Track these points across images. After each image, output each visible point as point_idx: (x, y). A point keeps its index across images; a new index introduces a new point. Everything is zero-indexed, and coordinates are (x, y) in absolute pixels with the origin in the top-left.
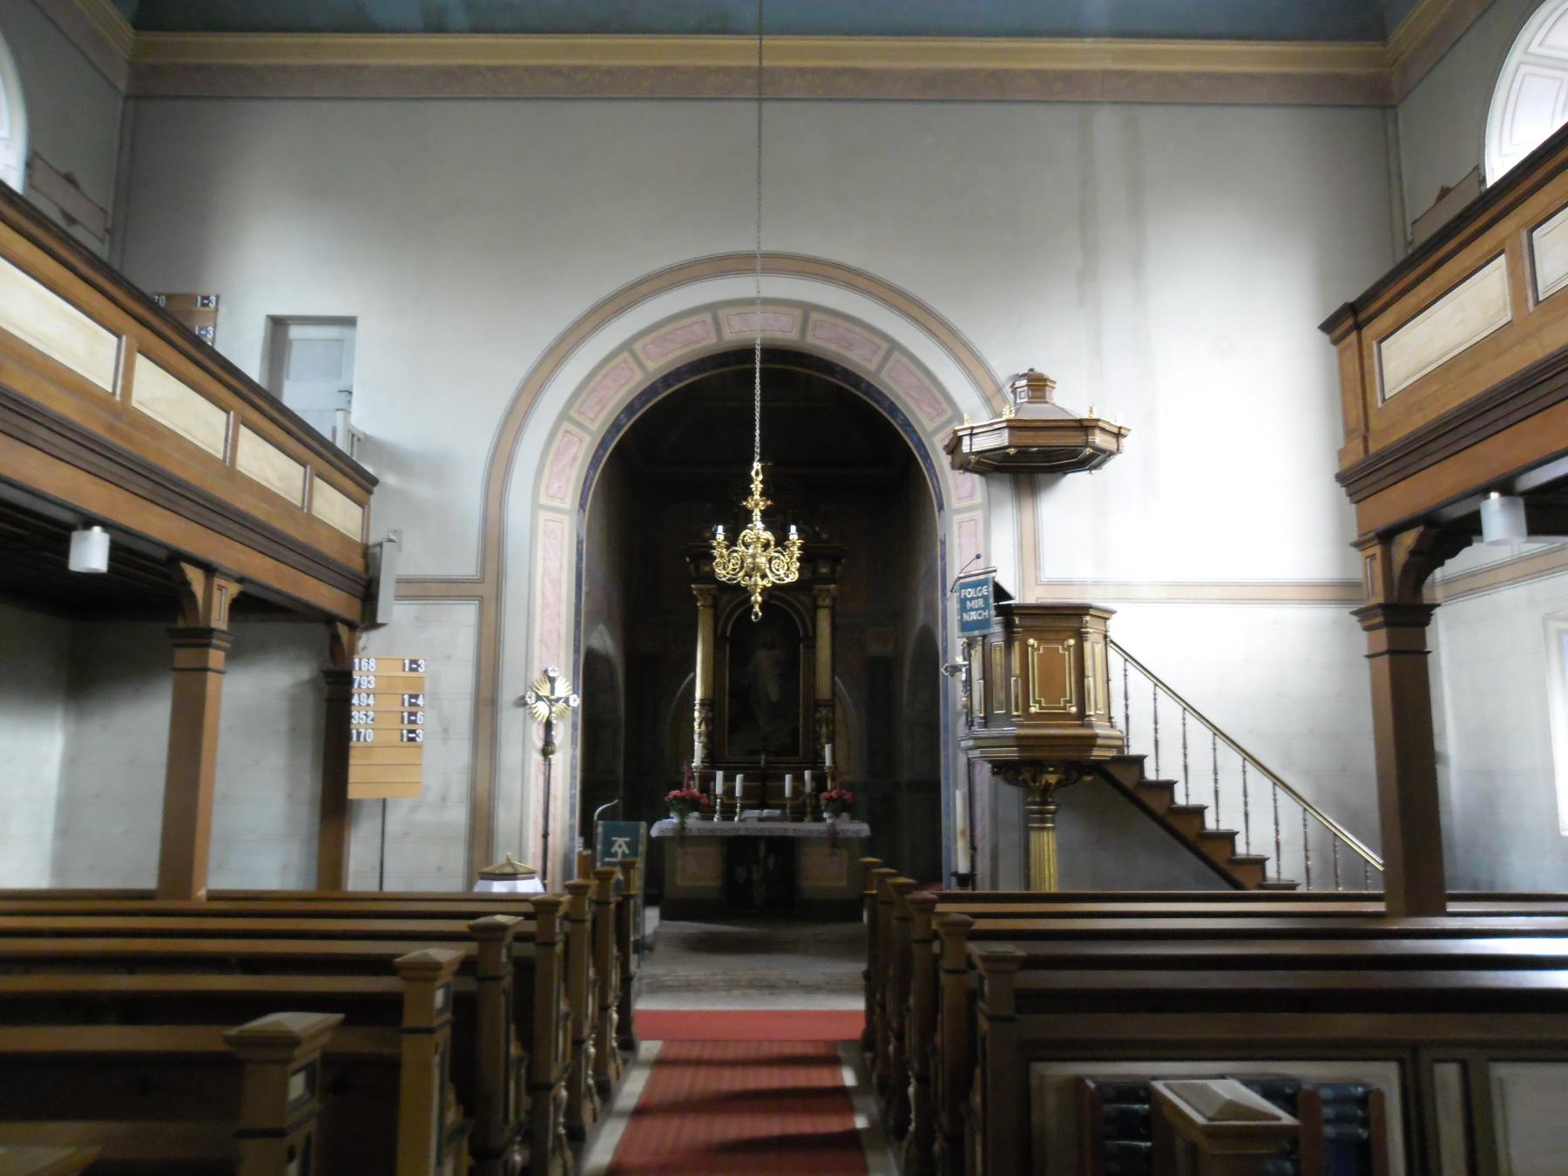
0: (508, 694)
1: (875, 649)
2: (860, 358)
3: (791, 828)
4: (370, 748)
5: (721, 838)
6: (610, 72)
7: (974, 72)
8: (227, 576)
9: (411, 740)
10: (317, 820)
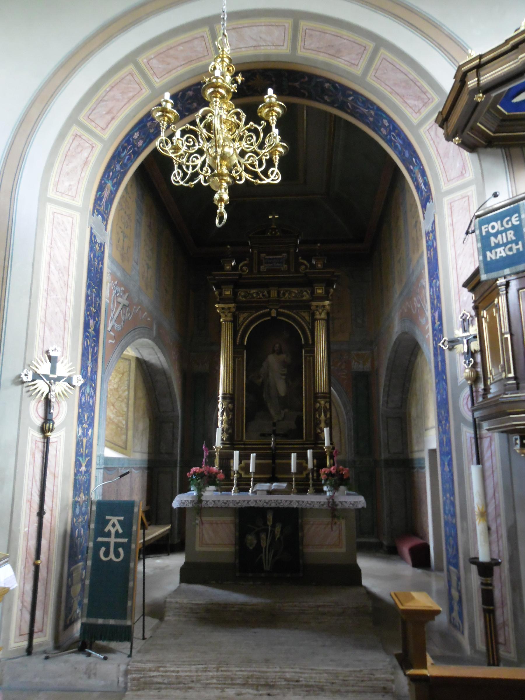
1: (357, 366)
3: (294, 500)
5: (234, 509)
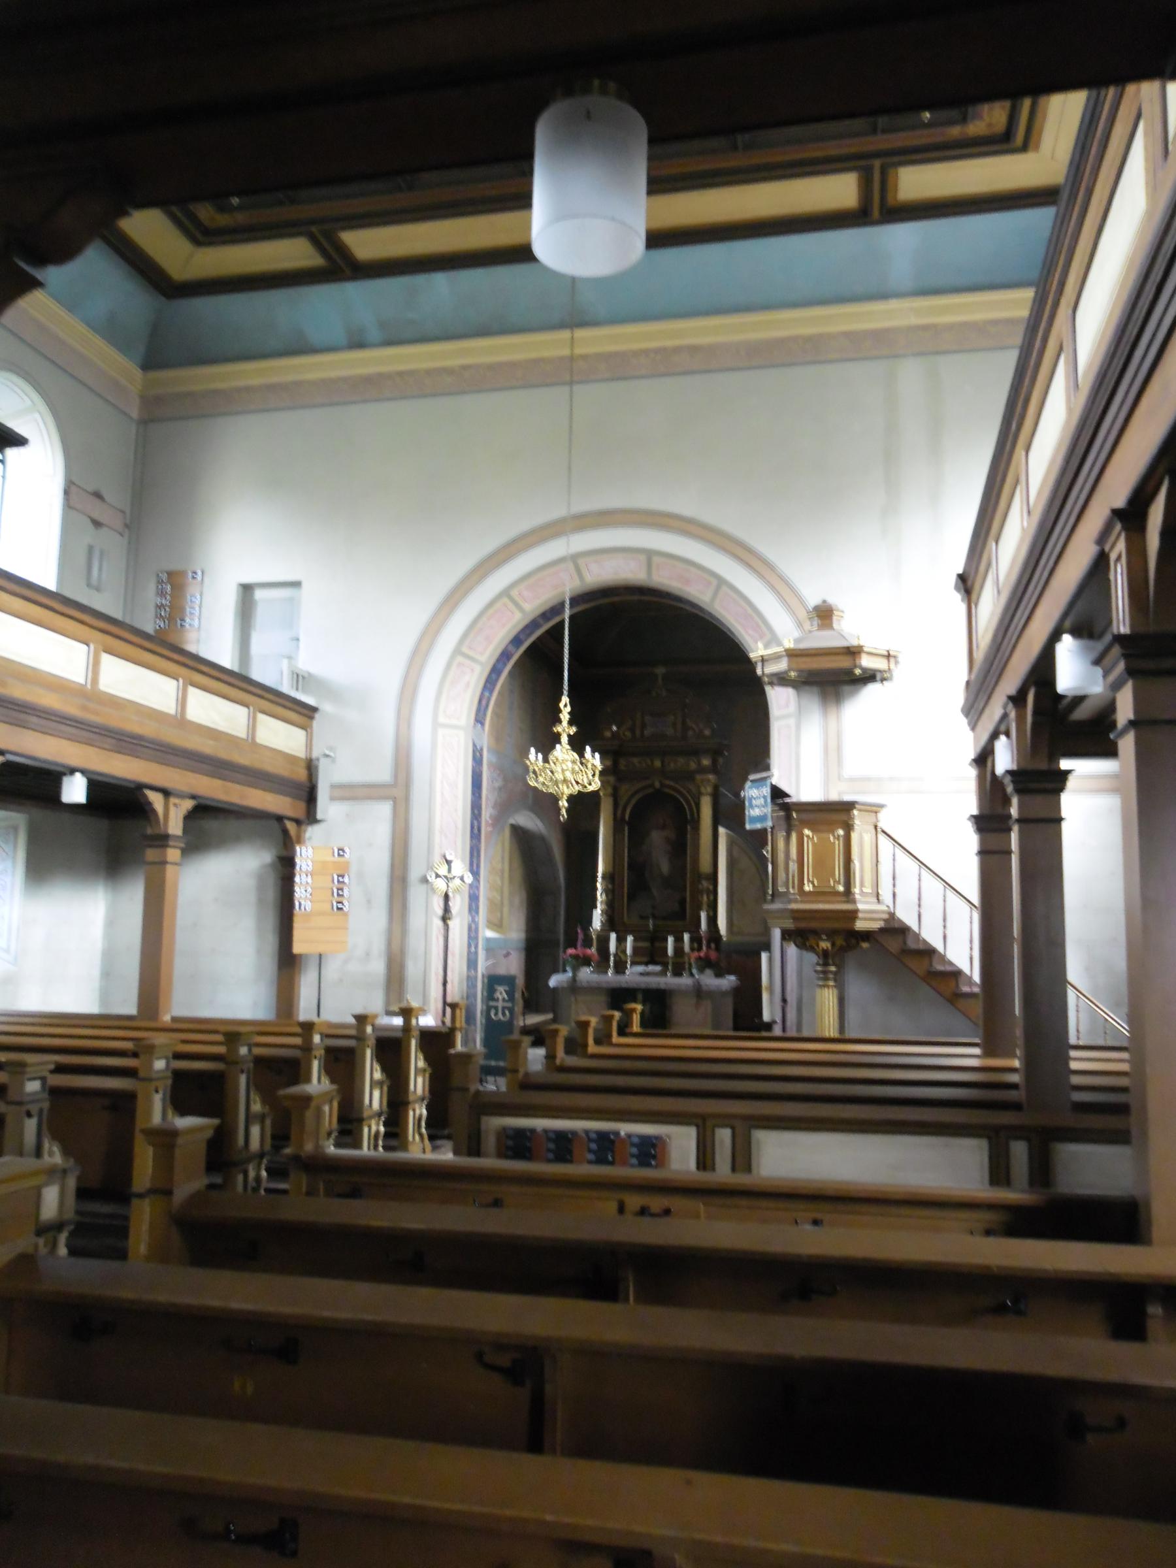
0: (415, 873)
2: (698, 593)
3: (669, 981)
4: (308, 916)
6: (491, 367)
7: (794, 339)
8: (181, 796)
9: (338, 909)
10: (275, 968)
